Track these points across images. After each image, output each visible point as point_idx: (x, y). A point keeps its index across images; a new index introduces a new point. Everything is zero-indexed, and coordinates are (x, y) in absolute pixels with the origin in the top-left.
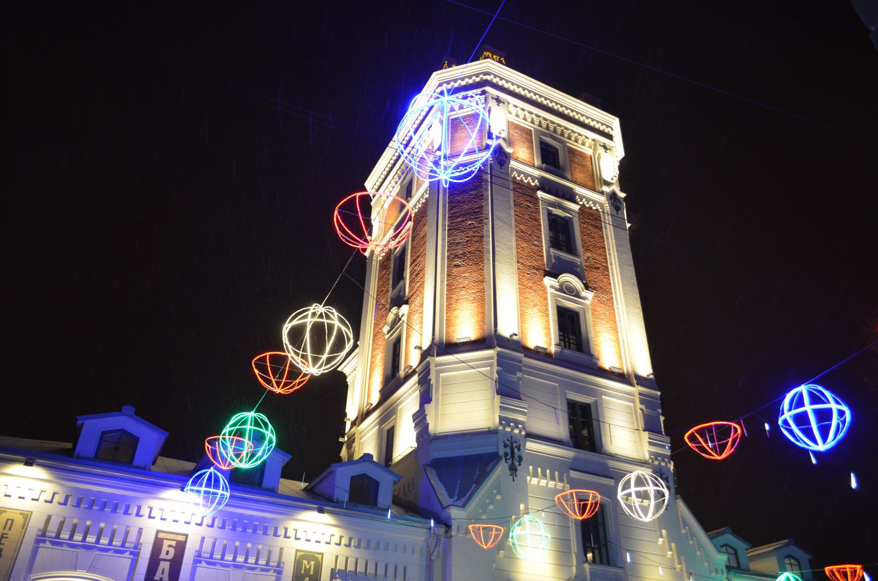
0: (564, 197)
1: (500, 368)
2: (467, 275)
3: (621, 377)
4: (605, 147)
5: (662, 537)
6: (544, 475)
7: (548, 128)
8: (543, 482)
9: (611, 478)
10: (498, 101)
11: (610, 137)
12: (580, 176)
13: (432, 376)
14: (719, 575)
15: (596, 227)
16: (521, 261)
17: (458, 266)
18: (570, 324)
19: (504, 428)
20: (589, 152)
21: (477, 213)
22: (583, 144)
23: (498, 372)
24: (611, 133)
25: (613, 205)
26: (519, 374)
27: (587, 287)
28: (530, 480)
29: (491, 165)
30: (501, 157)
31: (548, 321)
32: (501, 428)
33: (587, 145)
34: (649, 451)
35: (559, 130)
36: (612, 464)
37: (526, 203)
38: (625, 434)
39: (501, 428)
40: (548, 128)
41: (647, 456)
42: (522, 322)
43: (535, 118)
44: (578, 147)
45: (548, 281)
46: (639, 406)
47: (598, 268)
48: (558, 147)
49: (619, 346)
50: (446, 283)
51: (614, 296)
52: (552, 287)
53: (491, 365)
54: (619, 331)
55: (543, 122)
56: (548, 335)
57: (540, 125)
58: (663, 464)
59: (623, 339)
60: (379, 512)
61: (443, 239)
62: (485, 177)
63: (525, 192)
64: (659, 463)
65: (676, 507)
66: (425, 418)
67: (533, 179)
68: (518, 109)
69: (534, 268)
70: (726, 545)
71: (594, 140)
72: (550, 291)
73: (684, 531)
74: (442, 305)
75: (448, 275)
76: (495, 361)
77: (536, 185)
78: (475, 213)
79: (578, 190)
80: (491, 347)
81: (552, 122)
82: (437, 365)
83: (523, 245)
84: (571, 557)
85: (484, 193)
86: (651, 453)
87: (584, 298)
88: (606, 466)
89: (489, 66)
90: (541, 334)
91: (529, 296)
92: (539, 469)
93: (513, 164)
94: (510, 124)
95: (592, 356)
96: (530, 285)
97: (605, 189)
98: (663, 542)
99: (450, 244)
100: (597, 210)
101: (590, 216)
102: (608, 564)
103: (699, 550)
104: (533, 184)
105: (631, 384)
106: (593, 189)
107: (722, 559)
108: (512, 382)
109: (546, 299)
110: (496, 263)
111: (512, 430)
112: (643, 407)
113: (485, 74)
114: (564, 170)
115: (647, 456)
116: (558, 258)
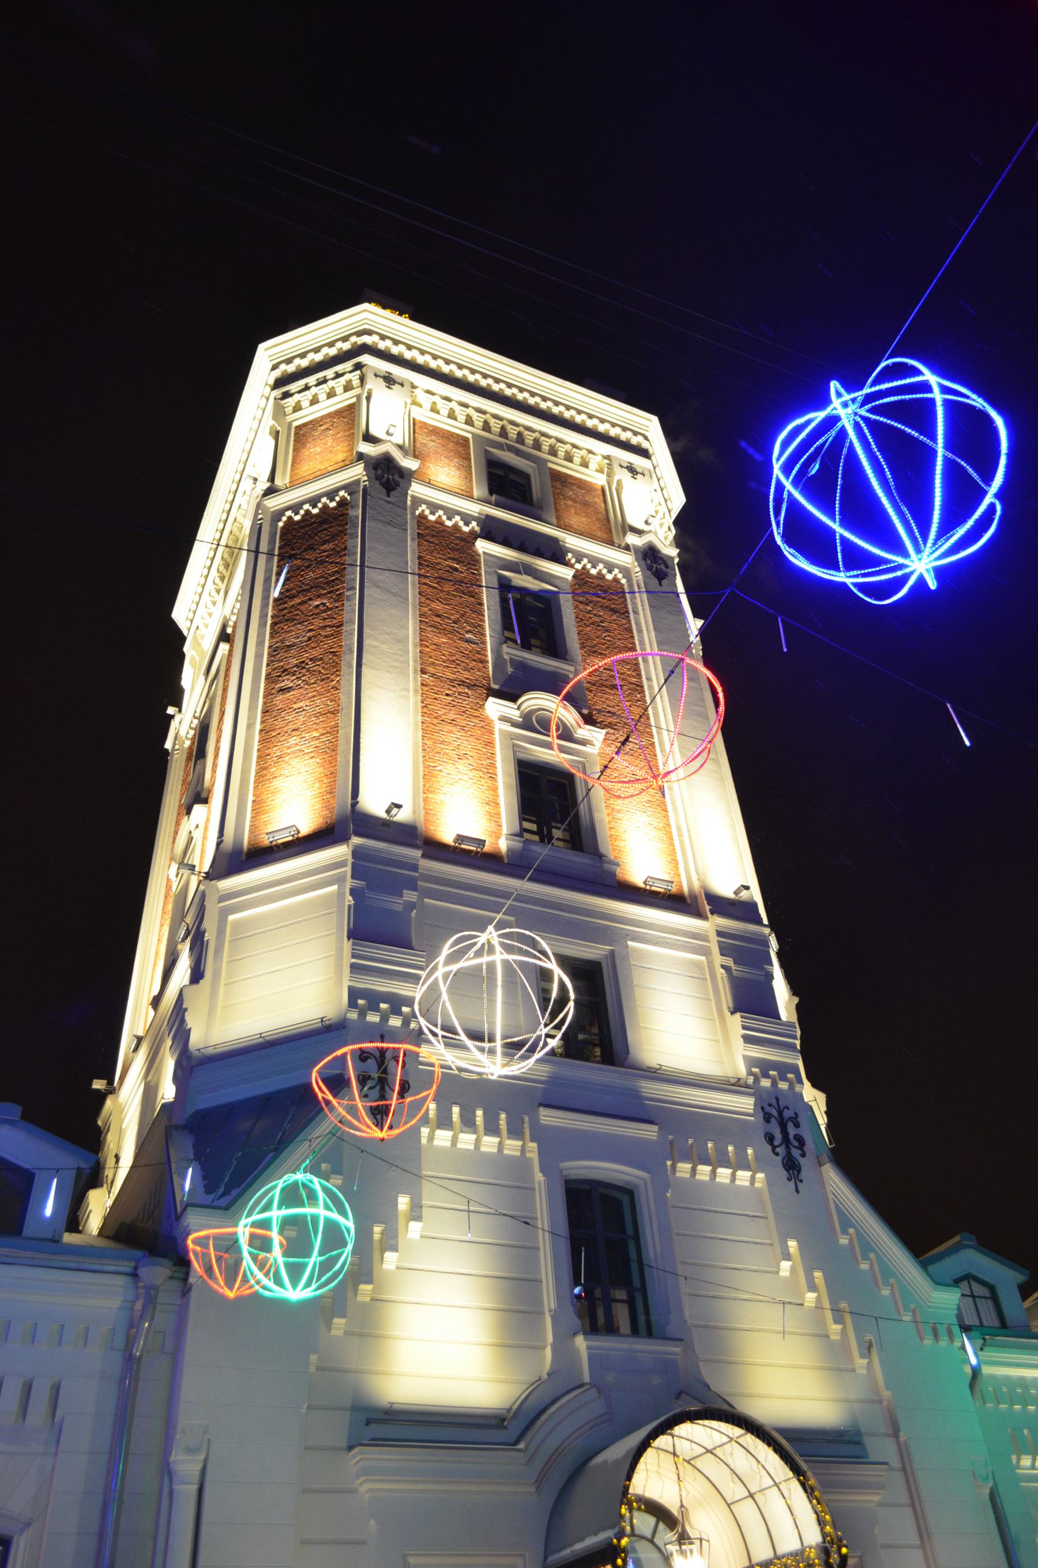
0: (539, 553)
1: (358, 883)
2: (304, 703)
3: (676, 901)
4: (632, 470)
5: (787, 1256)
6: (468, 1123)
7: (503, 433)
8: (467, 1140)
9: (651, 1122)
10: (389, 380)
11: (645, 453)
12: (575, 519)
13: (210, 926)
14: (944, 1342)
15: (614, 611)
16: (431, 669)
17: (289, 689)
18: (548, 798)
19: (362, 1014)
20: (599, 480)
21: (333, 586)
22: (585, 464)
23: (353, 892)
24: (645, 445)
25: (649, 568)
26: (410, 896)
27: (589, 720)
28: (431, 1138)
29: (365, 489)
30: (387, 475)
31: (495, 789)
32: (353, 1015)
33: (593, 465)
34: (745, 1057)
35: (529, 438)
36: (650, 1089)
37: (450, 563)
38: (686, 1026)
39: (353, 1015)
40: (503, 433)
41: (741, 1070)
42: (427, 790)
43: (475, 416)
44: (573, 470)
45: (495, 708)
46: (718, 959)
47: (614, 687)
48: (529, 471)
49: (671, 838)
50: (258, 727)
51: (656, 740)
52: (504, 719)
53: (339, 880)
54: (670, 808)
55: (492, 422)
56: (494, 816)
57: (486, 427)
58: (783, 1086)
59: (683, 821)
60: (71, 1261)
61: (260, 643)
62: (352, 513)
63: (444, 548)
64: (774, 1084)
65: (822, 1183)
66: (183, 1021)
67: (467, 519)
68: (437, 399)
69: (462, 683)
70: (968, 1277)
71: (608, 457)
72: (499, 726)
73: (844, 1241)
74: (245, 771)
75: (265, 712)
76: (348, 869)
77: (472, 532)
78: (328, 583)
79: (571, 541)
80: (344, 839)
81: (513, 423)
82: (223, 898)
83: (436, 640)
84: (543, 1323)
85: (350, 543)
86: (751, 1062)
87: (583, 742)
88: (636, 1095)
89: (369, 318)
90: (473, 808)
91: (450, 738)
92: (456, 1110)
93: (416, 489)
94: (415, 426)
95: (599, 856)
96: (452, 715)
97: (631, 539)
98: (793, 1269)
99: (274, 651)
100: (616, 580)
101: (599, 594)
102: (650, 1334)
103: (887, 1283)
104: (466, 529)
105: (699, 914)
106: (610, 542)
107: (947, 1301)
108: (391, 913)
109: (490, 744)
110: (364, 669)
111: (385, 1018)
112: (729, 962)
113: (359, 334)
114: (541, 508)
115: (741, 1070)
116: (521, 666)
